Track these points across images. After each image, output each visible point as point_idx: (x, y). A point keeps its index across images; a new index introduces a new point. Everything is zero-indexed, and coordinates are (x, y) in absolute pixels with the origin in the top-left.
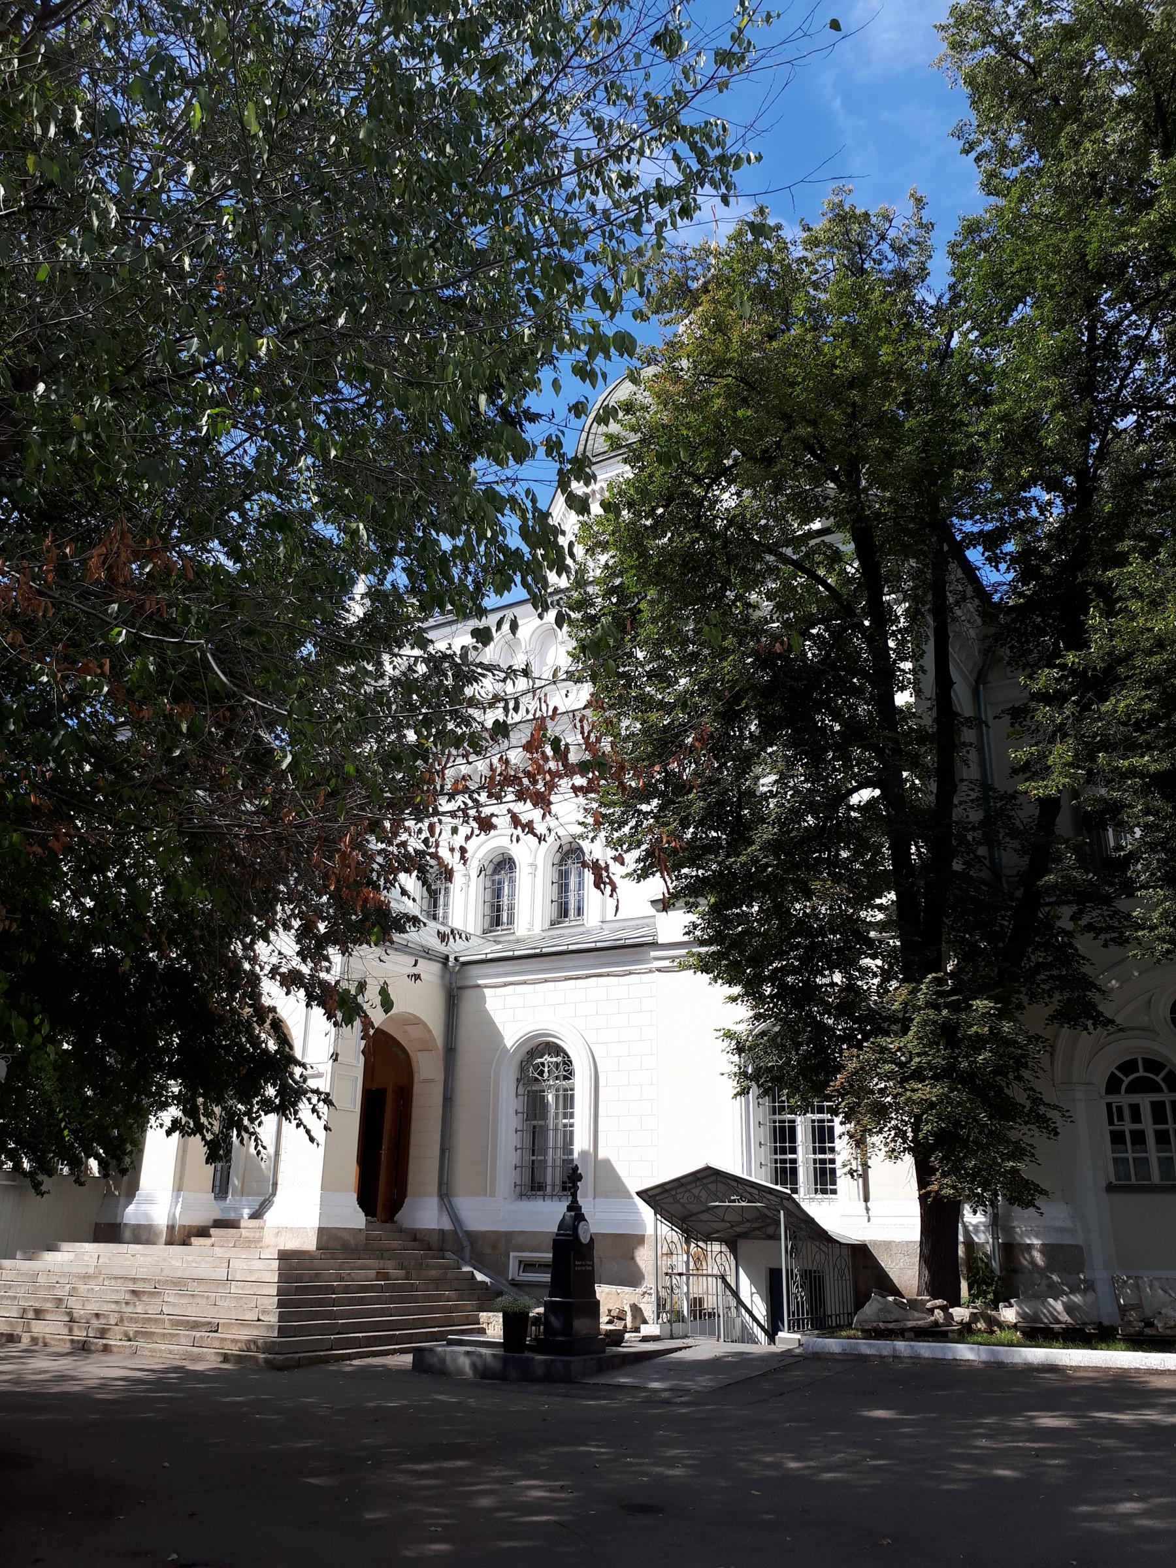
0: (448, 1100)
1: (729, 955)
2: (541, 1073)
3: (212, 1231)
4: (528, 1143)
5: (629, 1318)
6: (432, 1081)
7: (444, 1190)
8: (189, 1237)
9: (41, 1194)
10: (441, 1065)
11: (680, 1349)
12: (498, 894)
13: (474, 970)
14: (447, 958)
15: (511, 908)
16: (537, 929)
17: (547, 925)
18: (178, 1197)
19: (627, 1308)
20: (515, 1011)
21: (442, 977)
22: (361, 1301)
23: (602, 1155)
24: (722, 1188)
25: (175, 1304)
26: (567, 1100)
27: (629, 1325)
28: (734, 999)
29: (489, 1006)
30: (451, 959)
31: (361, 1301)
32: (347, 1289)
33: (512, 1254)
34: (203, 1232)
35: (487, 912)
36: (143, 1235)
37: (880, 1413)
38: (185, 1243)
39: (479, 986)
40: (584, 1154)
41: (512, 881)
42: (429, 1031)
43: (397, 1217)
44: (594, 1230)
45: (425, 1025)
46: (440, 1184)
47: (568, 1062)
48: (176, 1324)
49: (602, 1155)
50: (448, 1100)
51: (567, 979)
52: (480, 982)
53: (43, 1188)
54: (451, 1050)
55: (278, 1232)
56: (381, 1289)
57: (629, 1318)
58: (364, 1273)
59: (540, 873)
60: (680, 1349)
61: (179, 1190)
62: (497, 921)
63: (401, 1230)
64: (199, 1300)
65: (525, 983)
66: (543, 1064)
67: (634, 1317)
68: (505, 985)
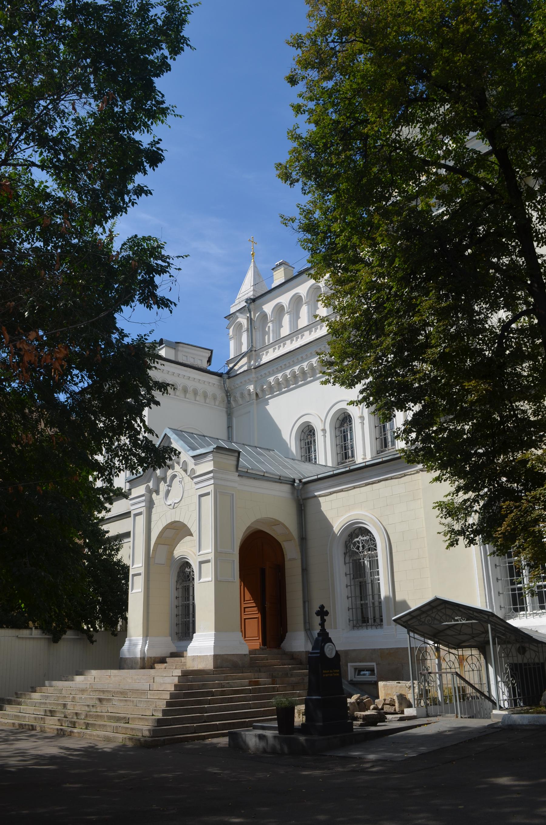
0: (305, 570)
1: (435, 451)
2: (358, 548)
3: (168, 660)
4: (358, 594)
5: (397, 705)
6: (294, 559)
7: (308, 627)
8: (154, 664)
9: (92, 642)
10: (298, 549)
11: (420, 726)
12: (345, 438)
13: (311, 487)
14: (294, 481)
15: (352, 447)
16: (369, 457)
17: (375, 454)
18: (146, 640)
19: (395, 698)
20: (339, 509)
21: (293, 493)
22: (231, 700)
23: (398, 598)
24: (449, 612)
25: (118, 707)
26: (374, 563)
27: (397, 710)
28: (438, 479)
29: (324, 508)
30: (297, 481)
31: (231, 700)
32: (223, 693)
33: (349, 664)
34: (162, 660)
35: (303, 445)
36: (120, 663)
37: (504, 781)
38: (152, 667)
39: (315, 496)
40: (387, 598)
41: (351, 429)
42: (287, 528)
43: (282, 644)
44: (340, 647)
45: (283, 524)
46: (305, 623)
47: (373, 539)
48: (110, 718)
49: (398, 598)
50: (305, 570)
51: (367, 484)
52: (316, 494)
53: (94, 639)
54: (303, 539)
55: (194, 658)
56: (250, 691)
57: (397, 705)
58: (240, 682)
59: (366, 421)
60: (420, 726)
61: (147, 636)
62: (346, 456)
63: (285, 653)
64: (129, 703)
65: (342, 491)
66: (358, 542)
67: (400, 704)
68: (331, 493)
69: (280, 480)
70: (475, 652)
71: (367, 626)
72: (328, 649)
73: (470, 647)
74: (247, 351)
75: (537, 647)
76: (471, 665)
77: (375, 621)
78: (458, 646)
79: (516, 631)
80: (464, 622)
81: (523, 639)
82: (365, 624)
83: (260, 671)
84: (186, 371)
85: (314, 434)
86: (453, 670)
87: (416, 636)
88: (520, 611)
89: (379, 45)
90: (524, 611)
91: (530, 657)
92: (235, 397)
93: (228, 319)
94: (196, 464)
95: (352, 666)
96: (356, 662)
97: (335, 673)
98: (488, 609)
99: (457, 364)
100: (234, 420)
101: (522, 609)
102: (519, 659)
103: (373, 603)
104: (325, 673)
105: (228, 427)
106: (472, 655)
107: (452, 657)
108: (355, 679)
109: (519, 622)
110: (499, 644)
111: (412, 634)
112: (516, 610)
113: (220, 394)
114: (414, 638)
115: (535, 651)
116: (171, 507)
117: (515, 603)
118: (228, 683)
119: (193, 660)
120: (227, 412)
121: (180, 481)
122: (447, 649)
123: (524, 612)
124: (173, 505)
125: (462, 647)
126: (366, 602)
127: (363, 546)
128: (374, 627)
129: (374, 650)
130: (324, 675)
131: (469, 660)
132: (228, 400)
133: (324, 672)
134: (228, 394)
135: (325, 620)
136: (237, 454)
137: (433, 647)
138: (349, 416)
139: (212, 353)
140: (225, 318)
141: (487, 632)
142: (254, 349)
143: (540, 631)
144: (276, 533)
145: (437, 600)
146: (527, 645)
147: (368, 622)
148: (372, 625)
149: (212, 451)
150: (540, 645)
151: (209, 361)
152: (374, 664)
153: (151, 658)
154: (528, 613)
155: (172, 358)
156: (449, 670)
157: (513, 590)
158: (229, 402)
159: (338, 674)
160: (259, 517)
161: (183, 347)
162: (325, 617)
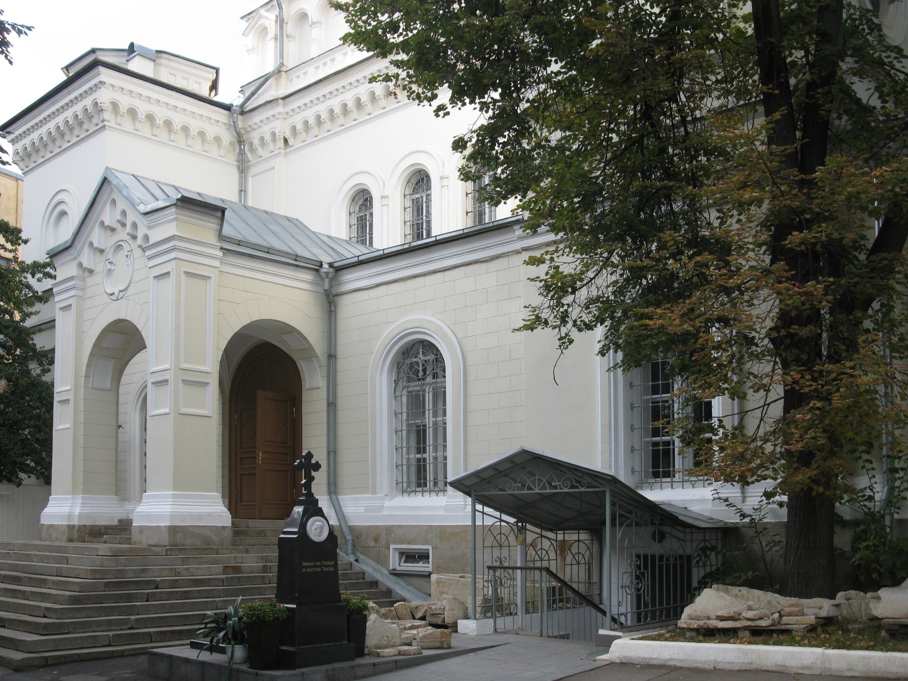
31: (186, 595)
32: (174, 584)
33: (392, 546)
46: (329, 484)
69: (296, 262)
70: (584, 536)
71: (423, 492)
72: (314, 527)
73: (578, 528)
74: (273, 71)
75: (684, 532)
76: (576, 557)
77: (435, 484)
78: (555, 527)
79: (652, 507)
80: (566, 490)
81: (664, 519)
82: (420, 489)
83: (247, 551)
84: (170, 96)
85: (371, 204)
86: (545, 564)
87: (487, 510)
88: (664, 477)
89: (668, 632)
90: (669, 476)
91: (671, 547)
92: (251, 144)
93: (247, 21)
94: (149, 228)
95: (396, 549)
96: (402, 543)
97: (327, 566)
98: (612, 472)
99: (613, 182)
100: (250, 180)
101: (667, 474)
102: (656, 549)
103: (435, 458)
104: (307, 567)
105: (241, 191)
106: (579, 541)
107: (546, 544)
108: (398, 568)
109: (659, 494)
110: (621, 525)
111: (479, 507)
112: (656, 475)
113: (227, 137)
114: (483, 513)
115: (678, 539)
116: (113, 297)
117: (655, 464)
118: (187, 569)
119: (141, 531)
120: (238, 167)
121: (127, 256)
122: (539, 531)
123: (669, 480)
124: (116, 294)
125: (564, 529)
126: (424, 455)
127: (424, 371)
128: (433, 494)
129: (431, 526)
130: (304, 570)
131: (574, 550)
132: (240, 149)
133: (304, 564)
134: (240, 139)
135: (313, 478)
136: (219, 214)
137: (515, 528)
138: (428, 176)
139: (217, 73)
140: (242, 18)
141: (604, 506)
142: (284, 69)
143: (689, 508)
144: (289, 346)
145: (524, 452)
146: (667, 529)
147: (425, 485)
148: (430, 491)
149: (175, 205)
150: (688, 530)
151: (214, 86)
152: (430, 547)
153: (85, 526)
154: (674, 479)
155: (150, 75)
156: (538, 564)
157: (655, 444)
158: (242, 153)
159: (332, 569)
160: (255, 318)
161: (168, 59)
162: (313, 473)
